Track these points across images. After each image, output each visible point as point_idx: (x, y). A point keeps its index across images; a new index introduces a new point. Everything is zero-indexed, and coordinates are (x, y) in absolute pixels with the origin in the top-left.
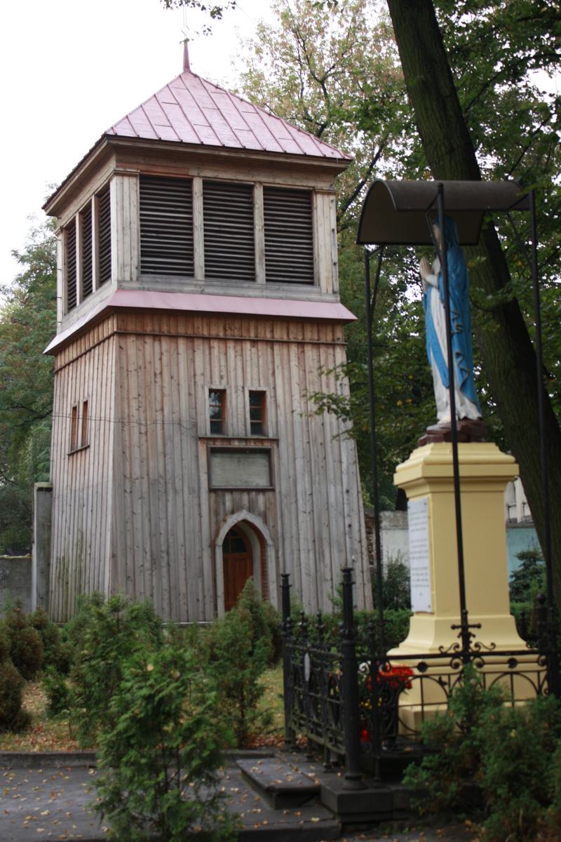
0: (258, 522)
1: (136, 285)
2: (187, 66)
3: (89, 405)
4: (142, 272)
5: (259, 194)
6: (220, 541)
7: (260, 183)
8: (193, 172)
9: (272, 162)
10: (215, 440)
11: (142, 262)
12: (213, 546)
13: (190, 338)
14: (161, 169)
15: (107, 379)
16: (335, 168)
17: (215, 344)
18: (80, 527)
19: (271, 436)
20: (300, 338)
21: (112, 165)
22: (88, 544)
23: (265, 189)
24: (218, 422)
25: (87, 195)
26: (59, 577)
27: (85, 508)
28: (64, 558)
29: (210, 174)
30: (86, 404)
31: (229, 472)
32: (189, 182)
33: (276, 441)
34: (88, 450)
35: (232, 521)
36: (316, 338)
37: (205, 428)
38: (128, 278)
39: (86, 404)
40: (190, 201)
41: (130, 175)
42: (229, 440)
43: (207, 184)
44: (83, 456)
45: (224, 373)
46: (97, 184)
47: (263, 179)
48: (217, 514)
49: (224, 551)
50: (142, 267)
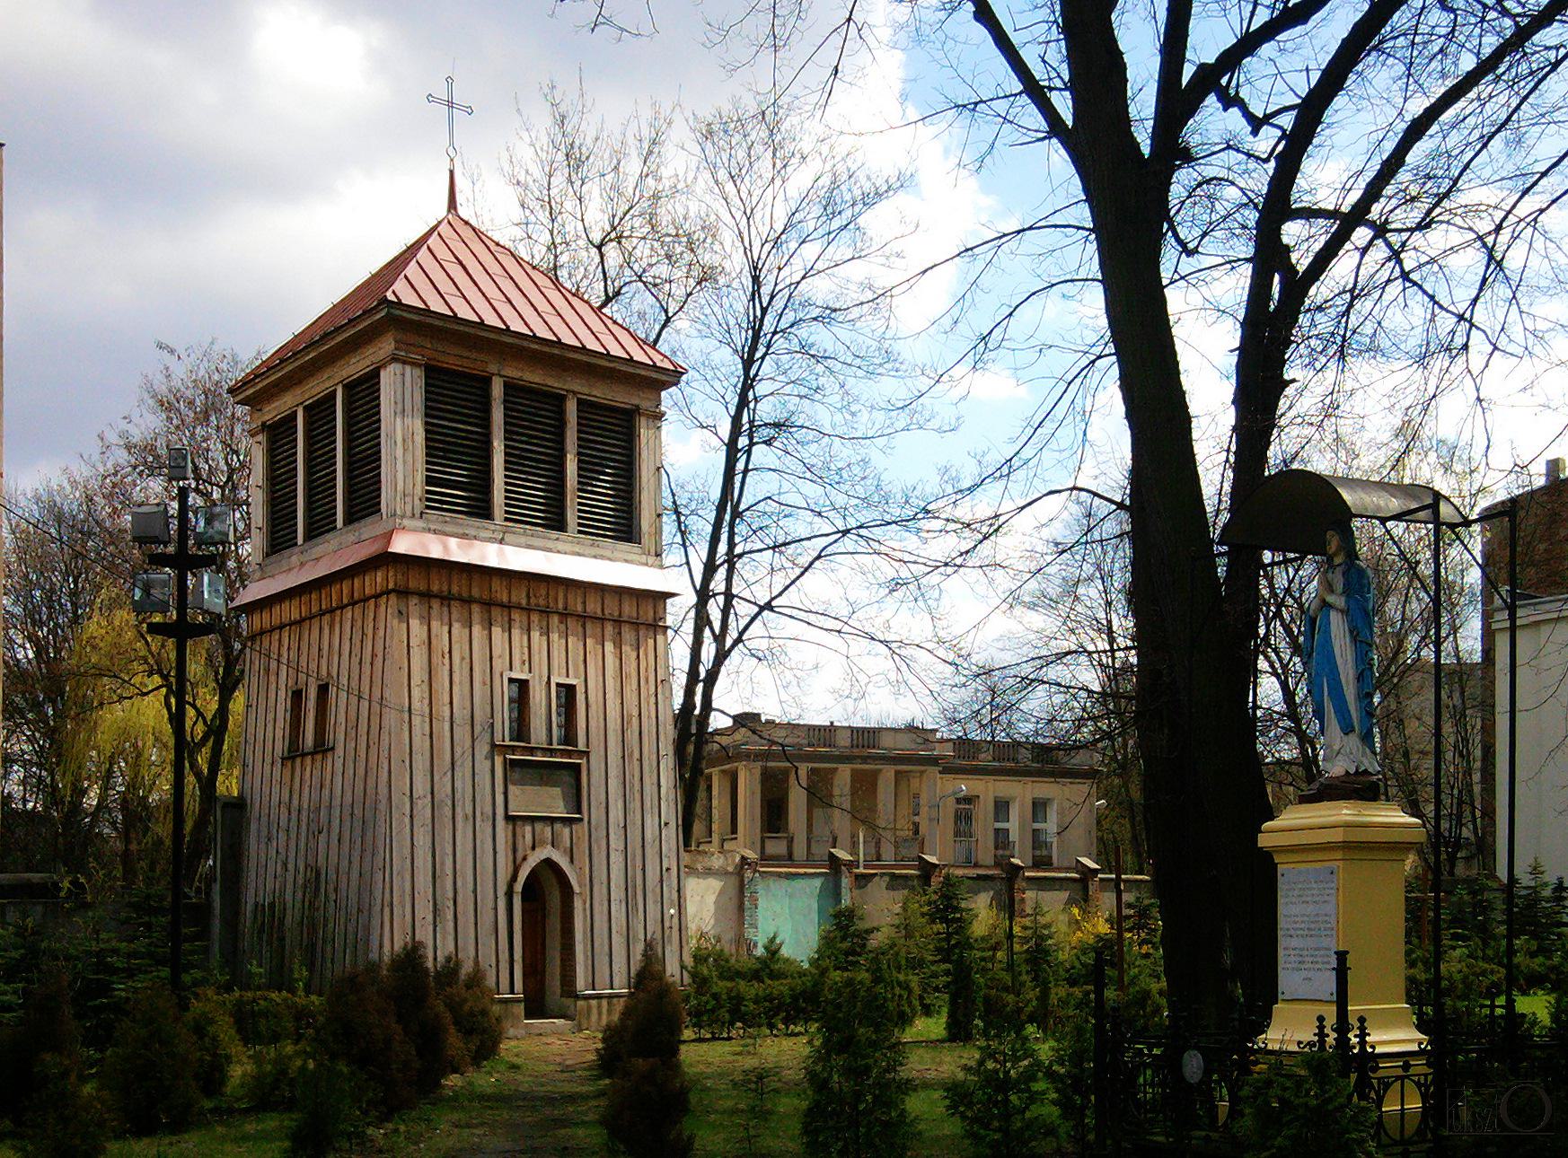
0: (563, 862)
1: (421, 524)
2: (452, 204)
3: (332, 691)
4: (428, 507)
5: (571, 408)
6: (519, 887)
7: (574, 393)
8: (493, 368)
9: (588, 364)
10: (513, 749)
11: (428, 492)
12: (510, 894)
13: (426, 596)
14: (453, 358)
15: (374, 655)
16: (656, 380)
17: (516, 615)
18: (311, 860)
19: (581, 747)
20: (423, 587)
21: (386, 346)
22: (331, 887)
23: (580, 402)
24: (521, 728)
25: (332, 381)
26: (261, 931)
27: (323, 838)
28: (272, 905)
29: (512, 372)
30: (323, 690)
31: (528, 799)
32: (487, 381)
33: (587, 754)
34: (329, 755)
35: (534, 860)
36: (445, 588)
37: (503, 734)
38: (409, 513)
39: (323, 690)
40: (487, 410)
41: (414, 364)
42: (532, 751)
43: (509, 387)
44: (318, 765)
45: (526, 657)
46: (355, 366)
47: (577, 388)
48: (515, 851)
49: (523, 901)
50: (428, 500)
